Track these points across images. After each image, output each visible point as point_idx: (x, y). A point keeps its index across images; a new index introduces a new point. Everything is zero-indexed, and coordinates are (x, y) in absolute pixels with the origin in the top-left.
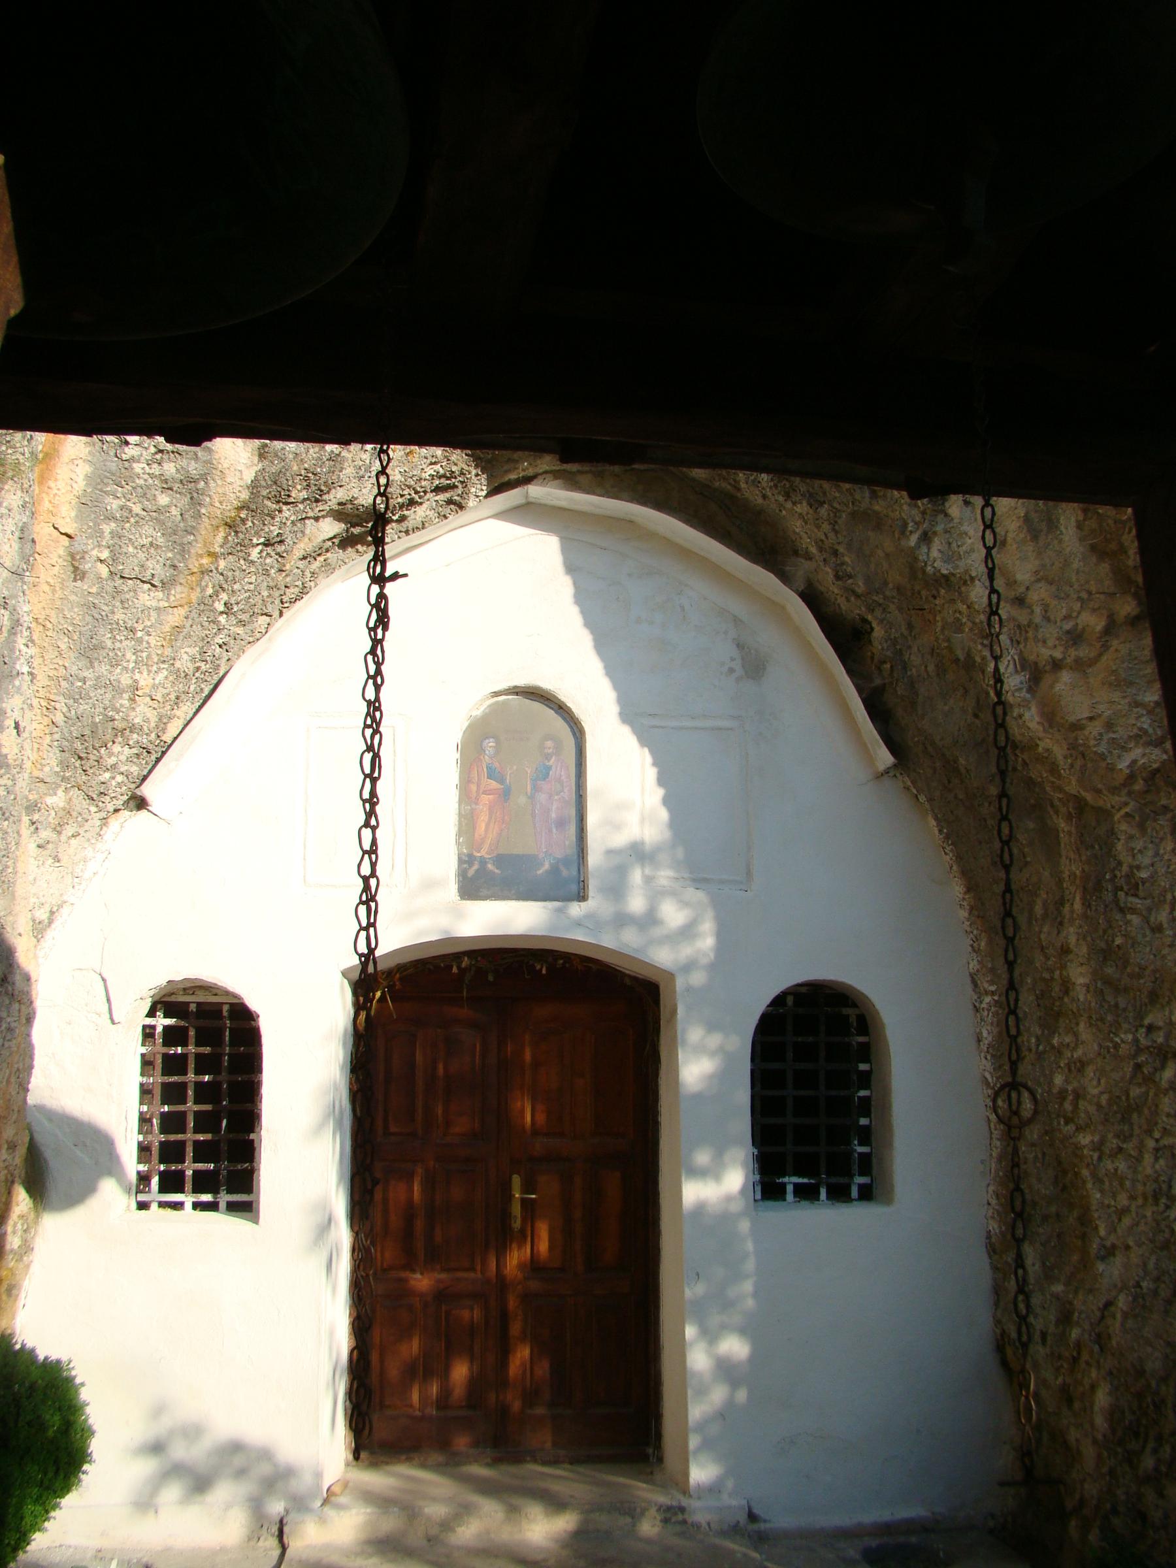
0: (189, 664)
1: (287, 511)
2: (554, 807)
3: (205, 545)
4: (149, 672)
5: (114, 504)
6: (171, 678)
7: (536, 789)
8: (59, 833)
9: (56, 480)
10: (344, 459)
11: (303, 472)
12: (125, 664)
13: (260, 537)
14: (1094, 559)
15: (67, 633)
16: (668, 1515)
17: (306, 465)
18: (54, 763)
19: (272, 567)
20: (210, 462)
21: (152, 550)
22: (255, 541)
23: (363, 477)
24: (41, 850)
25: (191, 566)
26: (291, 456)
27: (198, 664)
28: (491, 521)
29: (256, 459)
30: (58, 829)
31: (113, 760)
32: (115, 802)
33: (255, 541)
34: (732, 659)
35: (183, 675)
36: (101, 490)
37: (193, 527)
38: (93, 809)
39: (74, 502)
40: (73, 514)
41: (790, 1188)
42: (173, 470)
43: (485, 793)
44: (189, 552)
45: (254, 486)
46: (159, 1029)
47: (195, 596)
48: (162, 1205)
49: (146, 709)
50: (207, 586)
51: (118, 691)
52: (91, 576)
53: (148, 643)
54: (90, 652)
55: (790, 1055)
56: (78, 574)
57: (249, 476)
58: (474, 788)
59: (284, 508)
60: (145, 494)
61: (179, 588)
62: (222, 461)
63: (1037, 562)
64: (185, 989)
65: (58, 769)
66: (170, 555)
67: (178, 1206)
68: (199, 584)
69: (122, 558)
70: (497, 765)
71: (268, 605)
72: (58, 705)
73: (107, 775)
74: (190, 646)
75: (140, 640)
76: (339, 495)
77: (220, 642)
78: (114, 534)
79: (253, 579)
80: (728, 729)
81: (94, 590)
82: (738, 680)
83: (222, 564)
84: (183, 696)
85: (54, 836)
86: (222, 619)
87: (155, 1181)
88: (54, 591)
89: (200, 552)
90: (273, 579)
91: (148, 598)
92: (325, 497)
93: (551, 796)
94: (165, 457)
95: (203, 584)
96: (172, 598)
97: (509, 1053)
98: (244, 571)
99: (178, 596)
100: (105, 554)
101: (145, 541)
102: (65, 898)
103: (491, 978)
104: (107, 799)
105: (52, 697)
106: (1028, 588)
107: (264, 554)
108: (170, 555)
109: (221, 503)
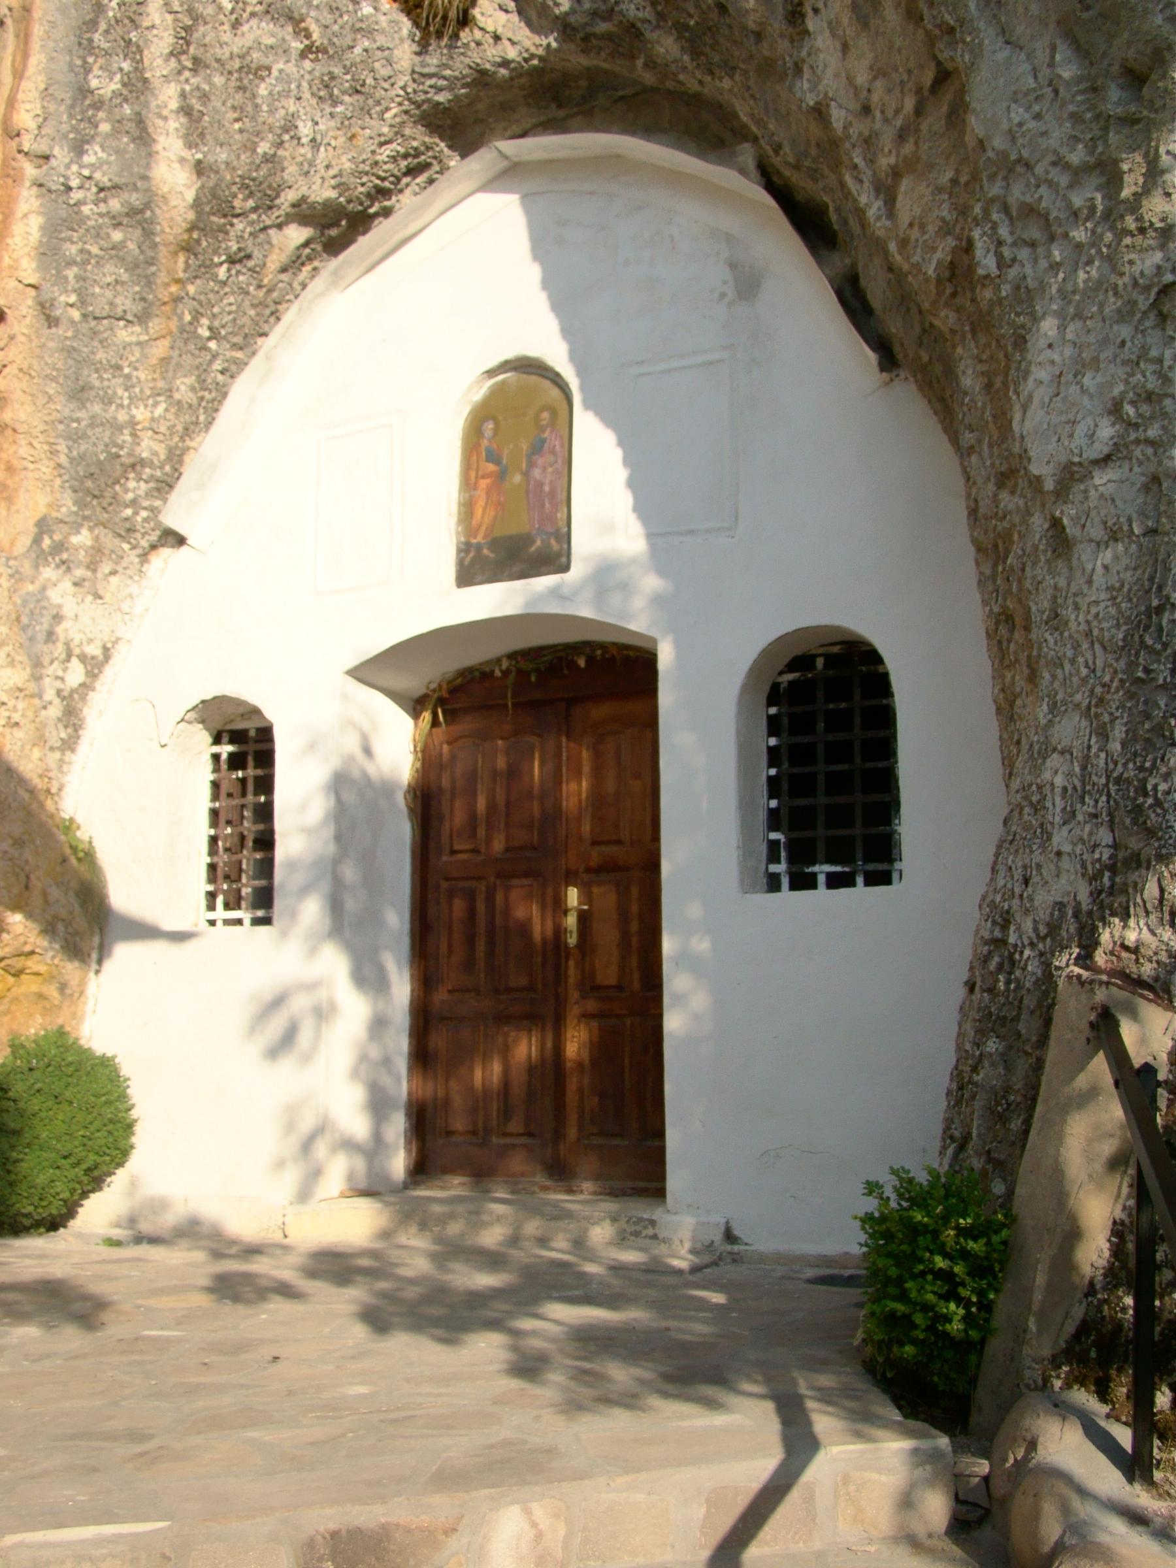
0: (191, 395)
1: (239, 224)
2: (547, 481)
3: (168, 273)
4: (146, 406)
5: (72, 250)
6: (173, 410)
7: (531, 464)
8: (95, 571)
9: (13, 236)
10: (283, 158)
11: (237, 180)
12: (119, 401)
13: (220, 255)
14: (911, 27)
15: (54, 379)
16: (638, 1228)
17: (239, 172)
18: (70, 503)
19: (249, 284)
20: (148, 190)
21: (119, 288)
22: (216, 260)
23: (308, 172)
24: (77, 589)
25: (160, 296)
26: (223, 166)
27: (201, 394)
28: (480, 197)
29: (194, 177)
30: (93, 566)
31: (130, 496)
32: (147, 537)
33: (216, 260)
34: (725, 282)
35: (186, 406)
36: (57, 238)
37: (153, 258)
38: (126, 546)
39: (32, 254)
40: (34, 265)
41: (821, 879)
42: (118, 206)
43: (483, 477)
44: (155, 283)
45: (197, 204)
46: (224, 756)
47: (174, 325)
48: (227, 922)
49: (152, 443)
50: (183, 313)
51: (119, 428)
52: (64, 321)
53: (138, 378)
54: (79, 393)
55: (821, 726)
56: (52, 321)
57: (190, 196)
58: (473, 474)
59: (235, 221)
60: (98, 234)
61: (156, 321)
62: (161, 185)
63: (872, 55)
64: (242, 715)
65: (74, 509)
66: (137, 289)
67: (239, 922)
68: (174, 310)
69: (89, 299)
70: (495, 446)
71: (261, 323)
72: (59, 448)
73: (129, 512)
74: (185, 376)
75: (128, 377)
76: (290, 196)
77: (220, 368)
78: (78, 278)
79: (232, 300)
80: (718, 361)
81: (70, 334)
82: (730, 305)
83: (191, 289)
84: (192, 427)
85: (89, 574)
86: (213, 345)
87: (220, 900)
88: (30, 341)
89: (166, 280)
90: (254, 296)
91: (125, 334)
92: (277, 202)
93: (544, 469)
94: (108, 194)
95: (179, 311)
96: (151, 331)
97: (537, 755)
98: (218, 292)
99: (157, 328)
100: (73, 299)
101: (109, 279)
102: (118, 634)
103: (533, 679)
104: (138, 536)
105: (52, 440)
106: (869, 91)
107: (233, 272)
108: (137, 289)
109: (171, 228)
